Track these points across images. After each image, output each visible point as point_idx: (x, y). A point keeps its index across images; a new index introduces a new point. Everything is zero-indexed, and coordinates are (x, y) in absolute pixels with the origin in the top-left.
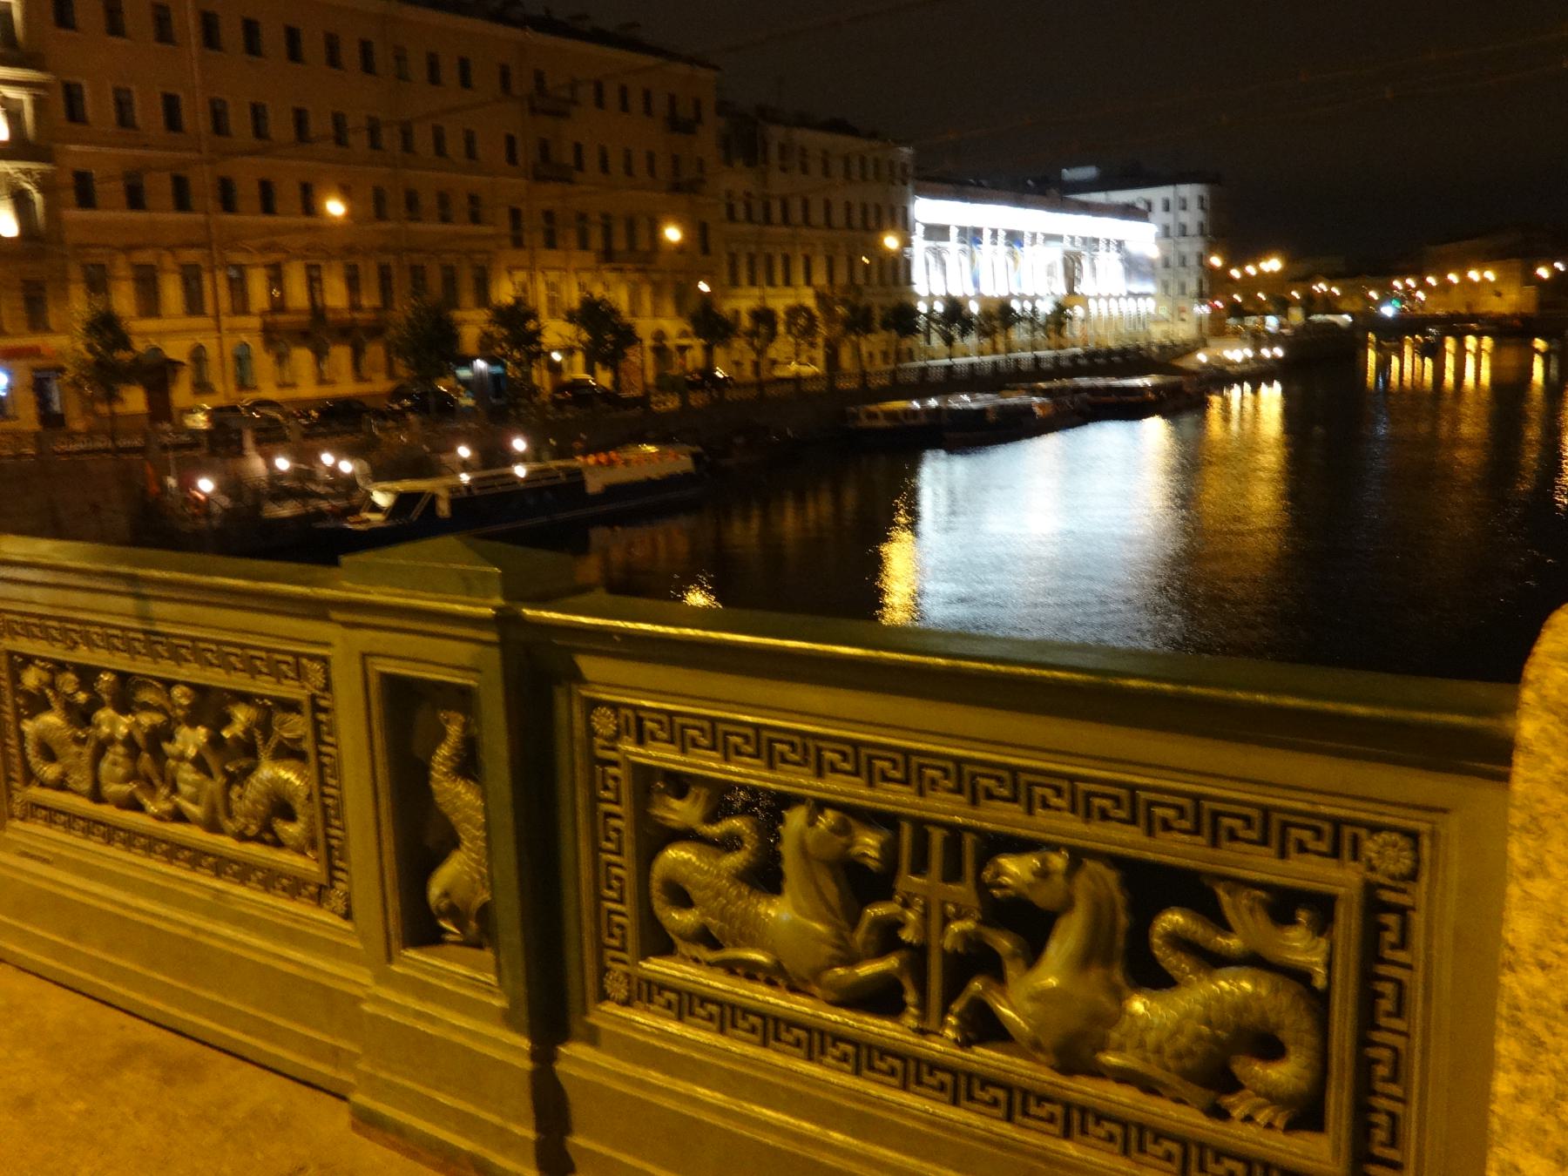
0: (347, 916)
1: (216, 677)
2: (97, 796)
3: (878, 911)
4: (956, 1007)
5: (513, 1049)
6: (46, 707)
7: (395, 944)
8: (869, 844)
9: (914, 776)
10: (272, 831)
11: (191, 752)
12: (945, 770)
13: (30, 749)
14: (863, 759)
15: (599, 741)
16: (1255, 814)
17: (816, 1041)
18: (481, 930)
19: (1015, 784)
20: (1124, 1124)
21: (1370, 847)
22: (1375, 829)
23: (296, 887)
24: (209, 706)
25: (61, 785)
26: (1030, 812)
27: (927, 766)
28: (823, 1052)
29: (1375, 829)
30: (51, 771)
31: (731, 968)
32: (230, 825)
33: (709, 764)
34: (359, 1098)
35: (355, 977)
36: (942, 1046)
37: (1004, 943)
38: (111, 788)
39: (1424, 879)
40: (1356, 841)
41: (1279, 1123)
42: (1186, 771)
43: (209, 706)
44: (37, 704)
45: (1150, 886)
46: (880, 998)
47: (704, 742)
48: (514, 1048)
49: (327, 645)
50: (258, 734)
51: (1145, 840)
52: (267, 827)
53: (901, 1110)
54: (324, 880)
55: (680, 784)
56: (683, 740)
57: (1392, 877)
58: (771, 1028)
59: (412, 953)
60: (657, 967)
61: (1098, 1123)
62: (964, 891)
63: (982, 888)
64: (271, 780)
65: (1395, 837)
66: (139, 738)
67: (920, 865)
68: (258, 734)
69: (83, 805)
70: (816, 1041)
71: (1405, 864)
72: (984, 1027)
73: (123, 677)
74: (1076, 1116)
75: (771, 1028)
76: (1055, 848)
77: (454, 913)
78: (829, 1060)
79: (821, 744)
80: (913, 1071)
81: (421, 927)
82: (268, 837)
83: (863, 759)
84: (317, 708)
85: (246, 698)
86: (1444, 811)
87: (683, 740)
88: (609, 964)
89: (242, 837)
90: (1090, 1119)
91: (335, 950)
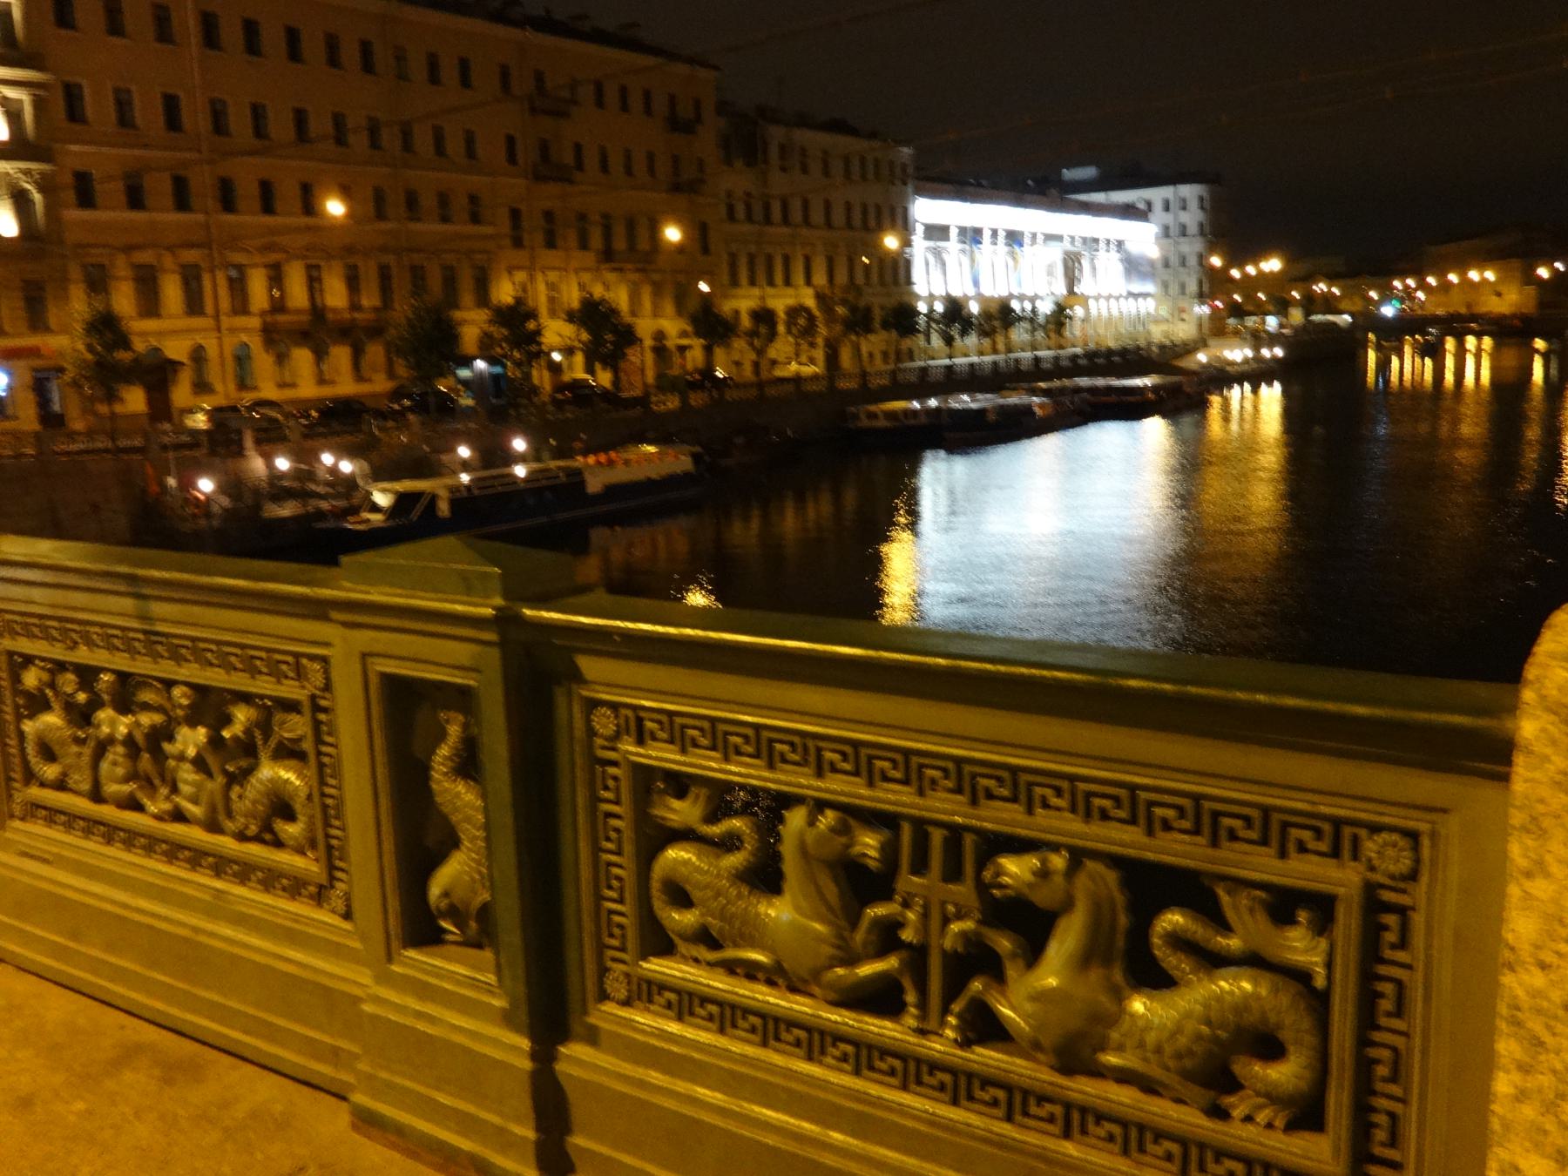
0: (347, 916)
1: (216, 677)
2: (97, 796)
3: (878, 911)
4: (956, 1007)
5: (513, 1049)
6: (46, 707)
7: (395, 944)
8: (869, 844)
9: (914, 776)
10: (272, 831)
11: (191, 752)
12: (945, 770)
13: (30, 749)
14: (863, 759)
15: (599, 741)
16: (1255, 814)
17: (816, 1041)
18: (481, 930)
19: (1015, 784)
20: (1124, 1124)
21: (1370, 847)
22: (1375, 829)
23: (296, 887)
24: (209, 706)
25: (61, 785)
26: (1030, 812)
27: (927, 766)
28: (823, 1052)
29: (1375, 829)
30: (51, 771)
31: (731, 968)
32: (230, 825)
33: (709, 764)
34: (359, 1098)
35: (355, 977)
36: (942, 1046)
37: (1004, 943)
38: (111, 788)
39: (1424, 879)
40: (1356, 841)
41: (1279, 1123)
42: (1186, 771)
43: (209, 706)
44: (37, 704)
45: (1150, 886)
46: (880, 998)
47: (704, 742)
48: (514, 1048)
49: (327, 645)
50: (258, 734)
51: (1145, 840)
52: (267, 827)
53: (901, 1110)
54: (324, 880)
55: (680, 784)
56: (683, 740)
57: (1392, 877)
58: (771, 1028)
59: (412, 953)
60: (657, 967)
61: (1098, 1123)
62: (964, 891)
63: (982, 888)
64: (271, 780)
65: (1395, 837)
66: (139, 738)
67: (920, 865)
68: (258, 734)
69: (83, 805)
70: (816, 1041)
71: (1405, 864)
72: (984, 1027)
73: (123, 677)
74: (1076, 1116)
75: (771, 1028)
76: (1055, 848)
77: (454, 913)
78: (829, 1060)
79: (821, 744)
80: (913, 1071)
81: (421, 927)
82: (268, 837)
83: (863, 759)
84: (317, 708)
85: (246, 698)
86: (1444, 811)
87: (683, 740)
88: (609, 964)
89: (242, 837)
90: (1090, 1119)
91: (335, 950)
